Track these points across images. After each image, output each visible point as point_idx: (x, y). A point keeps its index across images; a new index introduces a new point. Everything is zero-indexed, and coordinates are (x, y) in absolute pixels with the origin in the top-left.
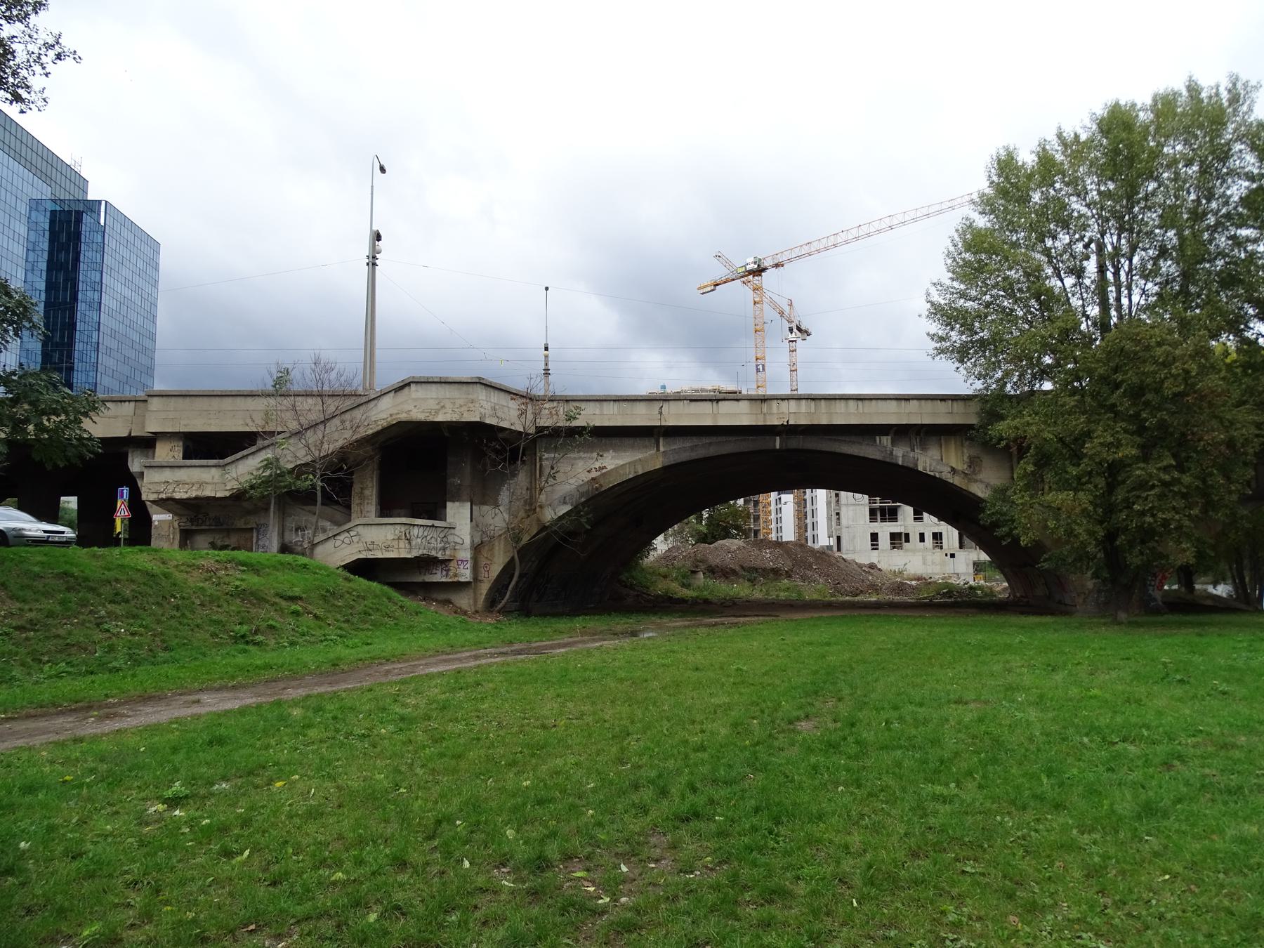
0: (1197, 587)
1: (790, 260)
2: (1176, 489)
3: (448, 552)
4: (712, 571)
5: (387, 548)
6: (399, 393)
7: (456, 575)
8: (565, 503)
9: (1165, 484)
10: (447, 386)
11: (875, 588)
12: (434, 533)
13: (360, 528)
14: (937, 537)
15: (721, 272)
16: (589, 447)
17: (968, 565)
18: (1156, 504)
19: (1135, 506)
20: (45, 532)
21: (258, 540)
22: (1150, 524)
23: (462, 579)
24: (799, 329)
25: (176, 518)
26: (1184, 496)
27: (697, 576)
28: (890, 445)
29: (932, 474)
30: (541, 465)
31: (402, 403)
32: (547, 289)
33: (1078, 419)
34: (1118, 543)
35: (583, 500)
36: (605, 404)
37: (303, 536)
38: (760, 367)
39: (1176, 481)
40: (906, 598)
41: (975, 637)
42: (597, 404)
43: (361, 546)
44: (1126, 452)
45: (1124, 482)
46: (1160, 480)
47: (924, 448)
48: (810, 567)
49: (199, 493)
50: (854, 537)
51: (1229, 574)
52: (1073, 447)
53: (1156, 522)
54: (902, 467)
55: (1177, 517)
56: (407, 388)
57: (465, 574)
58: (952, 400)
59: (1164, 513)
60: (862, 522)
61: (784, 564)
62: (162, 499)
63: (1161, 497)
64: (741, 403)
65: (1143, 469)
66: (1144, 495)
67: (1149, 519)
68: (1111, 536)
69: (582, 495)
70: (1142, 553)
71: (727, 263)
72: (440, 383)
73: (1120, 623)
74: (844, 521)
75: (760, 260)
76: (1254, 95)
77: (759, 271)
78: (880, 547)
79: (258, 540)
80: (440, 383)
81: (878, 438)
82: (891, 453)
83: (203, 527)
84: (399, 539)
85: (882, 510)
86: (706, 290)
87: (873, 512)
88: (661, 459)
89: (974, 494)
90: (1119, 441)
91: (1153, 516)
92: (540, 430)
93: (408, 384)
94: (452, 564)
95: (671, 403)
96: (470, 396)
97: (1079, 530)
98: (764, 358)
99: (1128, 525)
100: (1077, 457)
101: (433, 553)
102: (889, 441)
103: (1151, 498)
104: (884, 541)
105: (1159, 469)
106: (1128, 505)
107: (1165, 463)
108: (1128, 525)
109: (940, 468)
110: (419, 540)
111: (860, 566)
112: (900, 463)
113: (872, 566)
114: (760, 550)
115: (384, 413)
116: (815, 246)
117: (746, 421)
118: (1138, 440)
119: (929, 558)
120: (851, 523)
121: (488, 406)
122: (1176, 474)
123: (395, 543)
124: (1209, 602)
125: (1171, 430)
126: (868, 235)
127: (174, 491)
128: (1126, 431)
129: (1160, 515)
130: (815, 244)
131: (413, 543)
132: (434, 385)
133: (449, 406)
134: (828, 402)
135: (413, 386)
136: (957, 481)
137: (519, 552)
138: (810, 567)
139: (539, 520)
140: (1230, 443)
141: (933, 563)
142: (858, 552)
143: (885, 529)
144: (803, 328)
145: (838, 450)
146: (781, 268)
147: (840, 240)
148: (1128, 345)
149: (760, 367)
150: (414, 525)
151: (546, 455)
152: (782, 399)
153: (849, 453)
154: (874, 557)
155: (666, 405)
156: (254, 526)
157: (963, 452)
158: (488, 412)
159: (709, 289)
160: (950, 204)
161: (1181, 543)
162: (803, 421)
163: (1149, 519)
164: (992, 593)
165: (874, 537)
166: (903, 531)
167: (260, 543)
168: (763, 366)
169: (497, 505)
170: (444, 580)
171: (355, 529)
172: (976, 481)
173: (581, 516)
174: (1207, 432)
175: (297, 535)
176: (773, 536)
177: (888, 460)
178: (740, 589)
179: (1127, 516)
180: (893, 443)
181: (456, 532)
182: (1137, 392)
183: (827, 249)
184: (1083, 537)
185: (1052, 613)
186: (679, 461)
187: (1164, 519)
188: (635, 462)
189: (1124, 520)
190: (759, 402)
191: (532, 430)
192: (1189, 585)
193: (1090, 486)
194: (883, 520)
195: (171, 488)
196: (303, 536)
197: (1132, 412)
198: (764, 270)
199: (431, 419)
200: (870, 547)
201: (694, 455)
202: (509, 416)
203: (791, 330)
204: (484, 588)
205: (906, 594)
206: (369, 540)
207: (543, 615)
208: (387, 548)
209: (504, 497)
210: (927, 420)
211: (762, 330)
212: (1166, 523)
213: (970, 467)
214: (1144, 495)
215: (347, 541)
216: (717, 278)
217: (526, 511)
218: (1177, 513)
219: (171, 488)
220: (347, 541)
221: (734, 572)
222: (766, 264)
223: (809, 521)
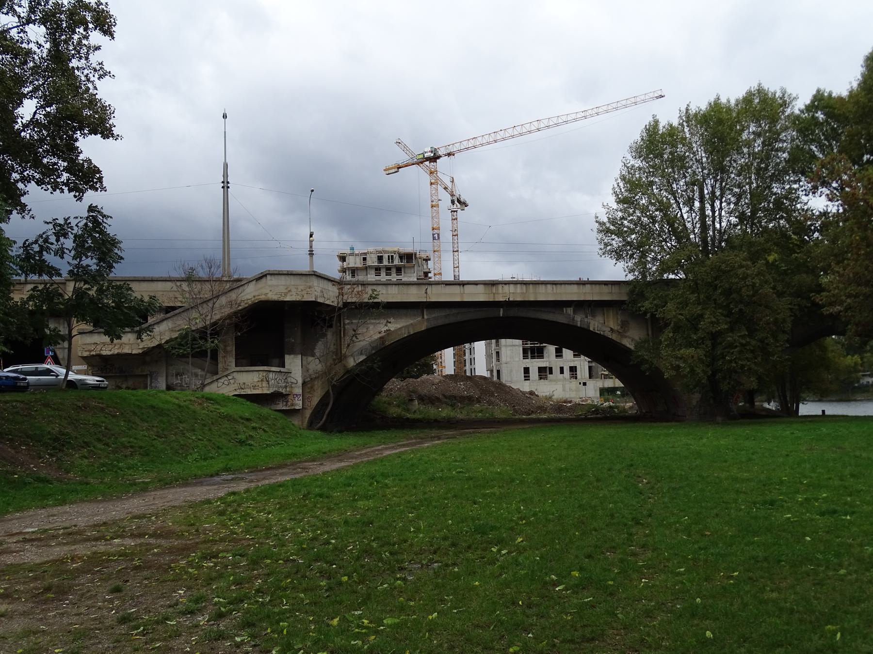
0: (756, 404)
1: (460, 151)
2: (748, 348)
3: (288, 389)
4: (422, 399)
5: (254, 387)
6: (259, 282)
7: (292, 405)
8: (361, 354)
9: (742, 345)
10: (292, 277)
11: (542, 409)
12: (280, 377)
13: (235, 374)
14: (573, 369)
15: (402, 157)
16: (380, 316)
17: (595, 391)
18: (738, 356)
19: (727, 358)
20: (97, 381)
21: (151, 382)
22: (734, 367)
23: (297, 408)
24: (459, 201)
25: (90, 368)
26: (752, 352)
27: (414, 403)
28: (572, 314)
29: (599, 332)
30: (344, 328)
31: (261, 288)
32: (312, 191)
33: (697, 307)
34: (717, 377)
35: (374, 352)
36: (389, 287)
37: (181, 380)
38: (436, 236)
39: (748, 343)
40: (567, 416)
41: (651, 432)
42: (397, 286)
43: (236, 386)
44: (722, 327)
45: (721, 344)
46: (740, 343)
47: (594, 316)
48: (493, 395)
49: (120, 351)
50: (511, 371)
51: (777, 394)
52: (694, 322)
53: (737, 366)
54: (580, 328)
55: (748, 363)
56: (264, 278)
57: (299, 405)
58: (612, 284)
59: (742, 362)
60: (517, 359)
61: (475, 393)
62: (93, 355)
63: (740, 352)
64: (478, 286)
65: (730, 337)
66: (732, 351)
67: (734, 365)
68: (714, 374)
69: (373, 348)
70: (729, 383)
71: (405, 148)
72: (288, 274)
73: (718, 423)
74: (504, 358)
75: (435, 149)
76: (794, 103)
77: (435, 158)
78: (531, 378)
79: (151, 382)
80: (288, 274)
81: (565, 309)
82: (573, 319)
83: (111, 374)
84: (262, 381)
85: (533, 350)
86: (391, 171)
87: (525, 351)
88: (425, 324)
89: (624, 345)
90: (718, 320)
91: (736, 363)
92: (346, 304)
93: (265, 275)
94: (290, 397)
95: (433, 286)
96: (308, 284)
97: (698, 370)
98: (439, 229)
99: (722, 368)
100: (696, 330)
101: (280, 390)
102: (572, 311)
103: (734, 353)
104: (534, 374)
105: (740, 336)
106: (723, 357)
107: (742, 333)
108: (722, 368)
109: (604, 329)
110: (273, 381)
111: (524, 393)
112: (579, 325)
113: (532, 393)
114: (456, 382)
115: (250, 294)
116: (480, 141)
117: (481, 298)
118: (728, 320)
119: (568, 386)
120: (508, 360)
121: (319, 290)
122: (748, 340)
123: (259, 384)
124: (764, 413)
125: (745, 314)
126: (521, 134)
127: (101, 350)
128: (722, 314)
129: (740, 362)
130: (480, 139)
131: (270, 383)
132: (283, 276)
133: (293, 290)
134: (534, 286)
135: (269, 277)
136: (614, 337)
137: (333, 386)
138: (493, 395)
139: (345, 366)
140: (776, 322)
141: (570, 389)
142: (514, 379)
143: (534, 365)
144: (462, 200)
145: (540, 317)
146: (452, 157)
147: (499, 137)
148: (723, 267)
149: (436, 236)
150: (270, 371)
151: (347, 321)
152: (505, 284)
153: (547, 319)
154: (526, 387)
155: (429, 288)
156: (148, 373)
157: (617, 319)
158: (319, 294)
159: (393, 171)
160: (583, 114)
161: (750, 378)
162: (519, 299)
163: (734, 365)
164: (624, 410)
165: (526, 370)
166: (548, 365)
167: (153, 385)
168: (438, 235)
169: (313, 355)
170: (284, 408)
171: (232, 375)
172: (626, 337)
173: (375, 363)
174: (764, 317)
175: (177, 379)
176: (468, 374)
177: (571, 324)
178: (444, 412)
179: (722, 363)
180: (574, 312)
181: (292, 375)
182: (728, 293)
183: (489, 143)
184: (701, 374)
185: (668, 421)
186: (437, 325)
187: (742, 365)
188: (409, 325)
189: (720, 365)
190: (490, 286)
191: (341, 305)
192: (752, 402)
193: (704, 346)
194: (533, 357)
195: (99, 347)
196: (181, 380)
197: (724, 304)
198: (439, 157)
199: (282, 299)
200: (523, 378)
201: (447, 321)
202: (329, 296)
203: (453, 202)
204: (308, 413)
205: (565, 413)
206: (241, 382)
207: (340, 432)
208: (254, 387)
209: (319, 349)
210: (596, 298)
211: (438, 206)
212: (743, 366)
213: (622, 327)
214: (732, 351)
215: (226, 383)
216: (400, 163)
217: (334, 360)
218: (748, 361)
219: (99, 347)
220: (226, 383)
221: (438, 399)
222: (440, 153)
223: (467, 357)
